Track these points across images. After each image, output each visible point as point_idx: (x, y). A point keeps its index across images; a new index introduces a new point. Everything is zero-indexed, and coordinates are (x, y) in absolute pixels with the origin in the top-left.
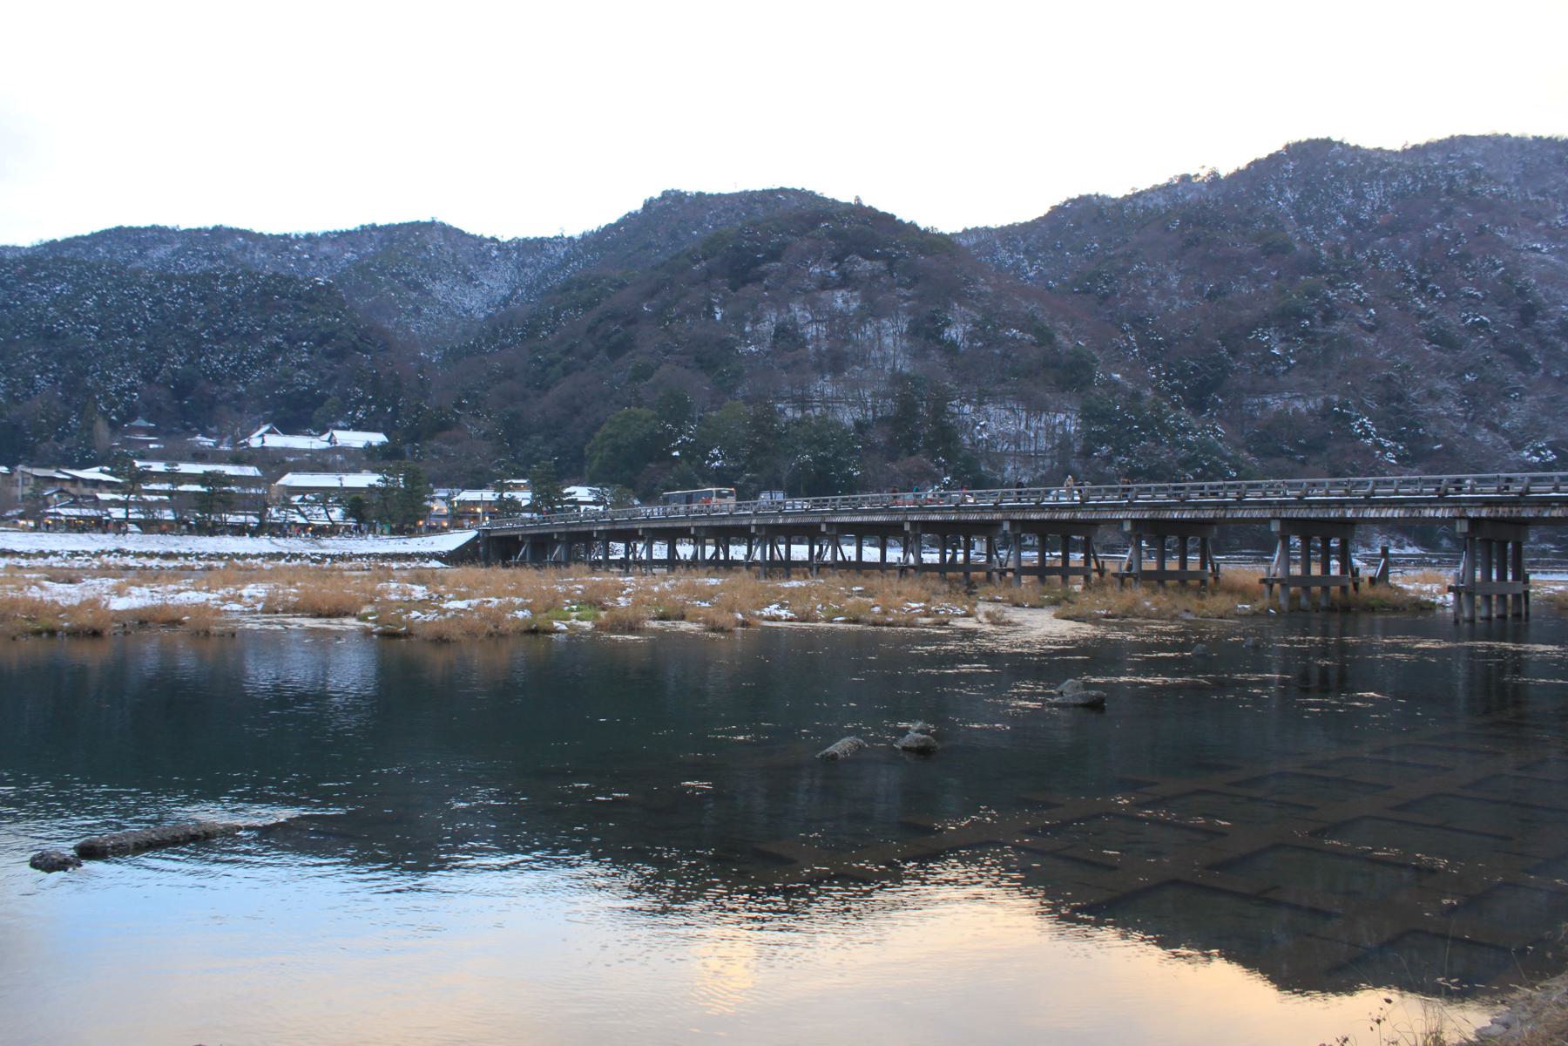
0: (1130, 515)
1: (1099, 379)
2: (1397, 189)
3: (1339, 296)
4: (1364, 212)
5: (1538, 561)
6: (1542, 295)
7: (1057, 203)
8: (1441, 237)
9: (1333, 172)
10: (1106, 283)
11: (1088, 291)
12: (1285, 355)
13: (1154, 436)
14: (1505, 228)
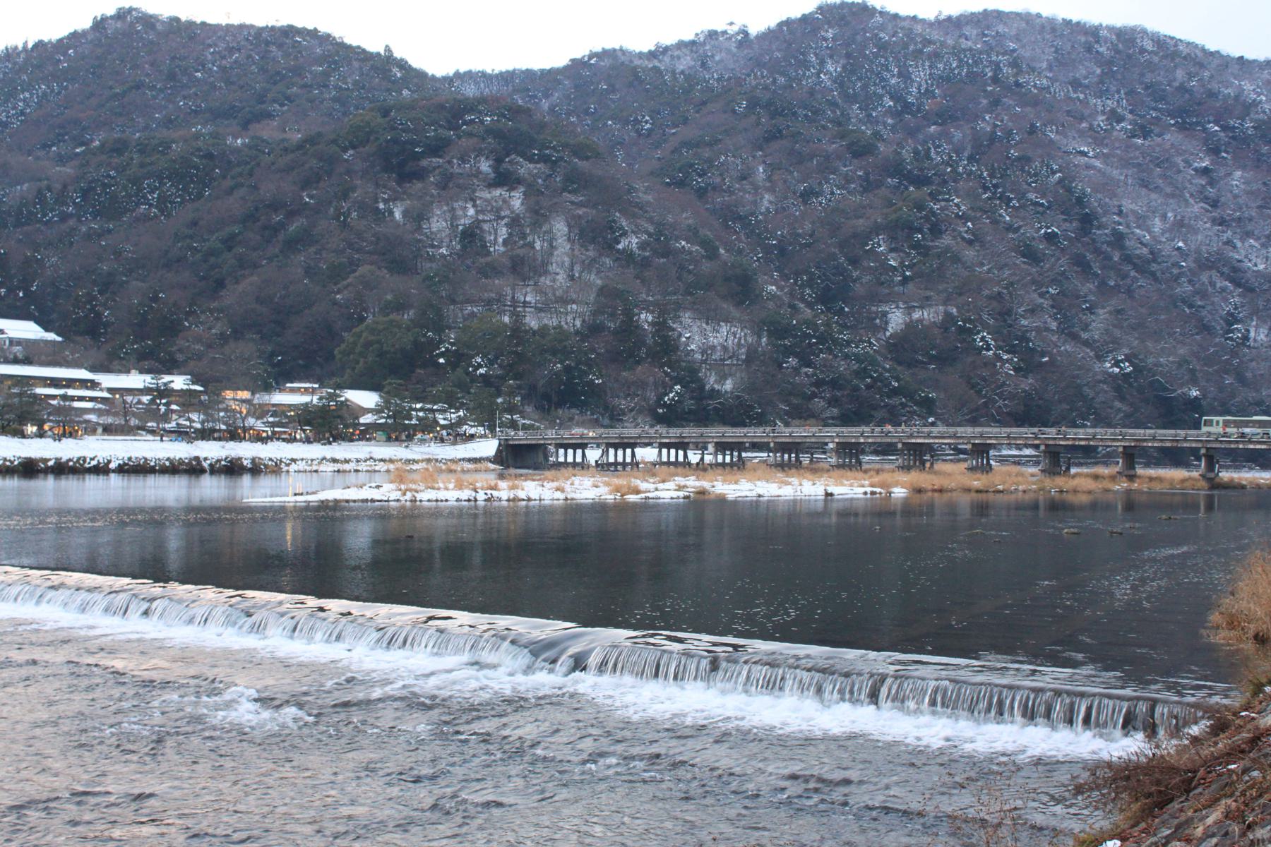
0: (1123, 444)
2: (943, 72)
3: (942, 209)
6: (1096, 204)
9: (875, 46)
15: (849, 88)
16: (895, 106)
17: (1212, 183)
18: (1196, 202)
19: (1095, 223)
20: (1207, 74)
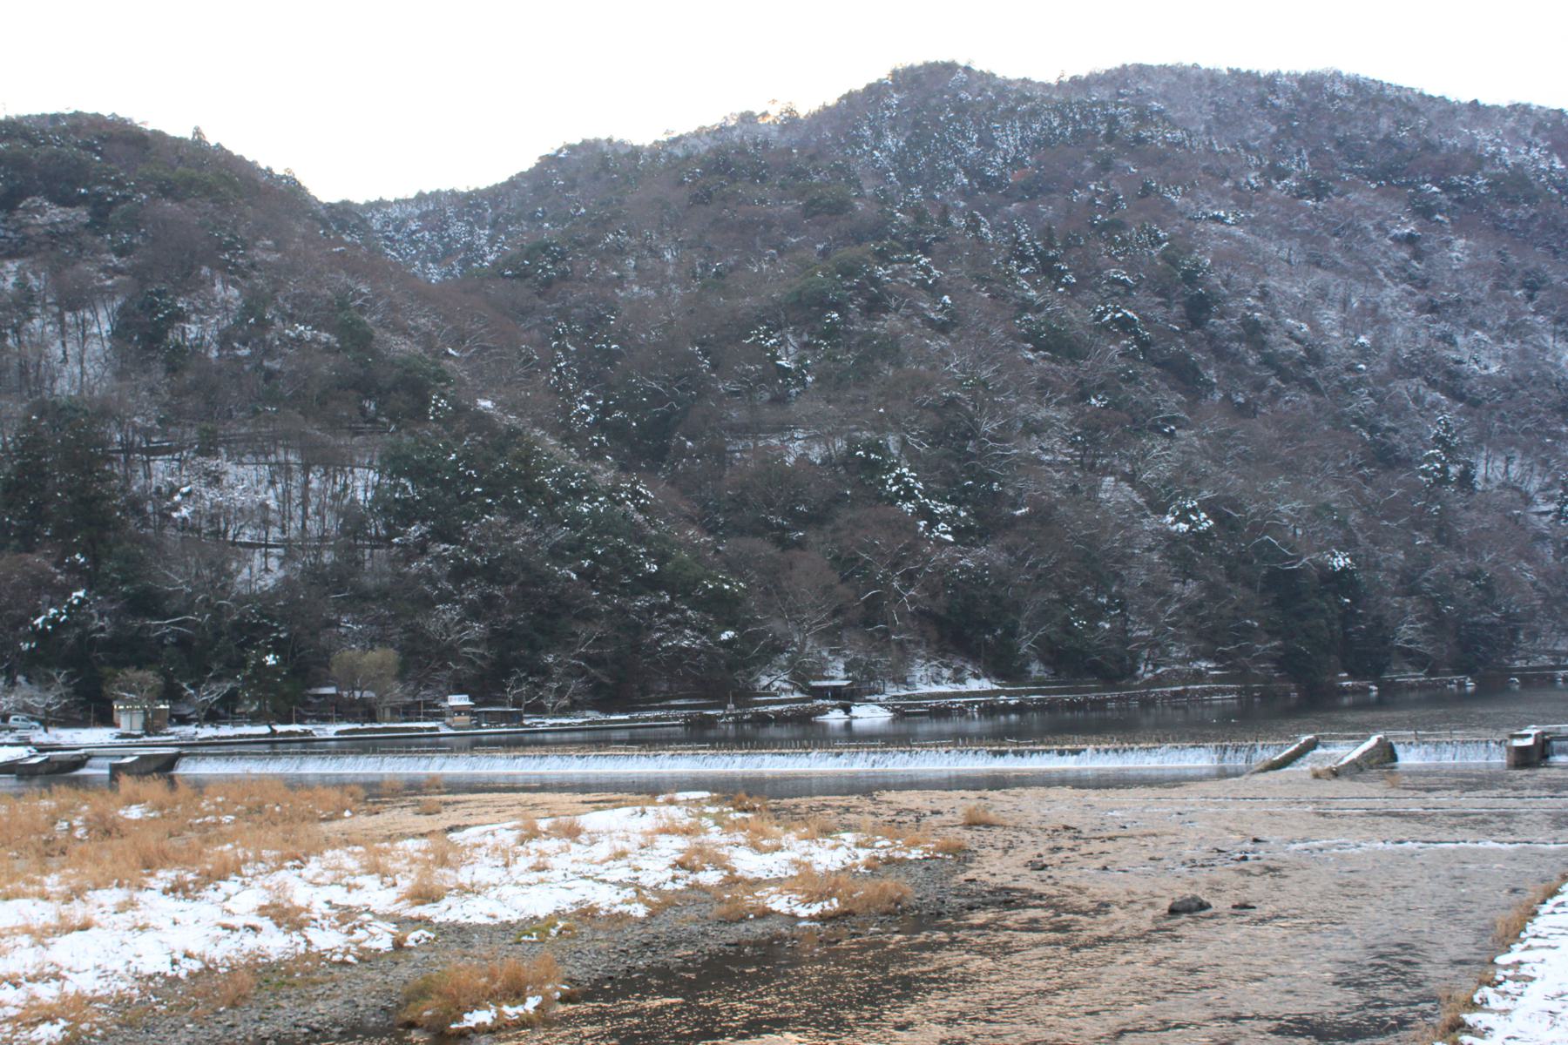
1: (438, 409)
2: (1040, 134)
3: (895, 275)
4: (991, 166)
5: (1186, 691)
7: (549, 150)
8: (1092, 201)
9: (952, 110)
10: (554, 262)
11: (522, 275)
12: (798, 370)
13: (509, 506)
14: (1180, 189)
15: (910, 166)
16: (970, 183)
17: (1418, 256)
18: (1396, 285)
19: (1215, 308)
20: (1422, 121)
